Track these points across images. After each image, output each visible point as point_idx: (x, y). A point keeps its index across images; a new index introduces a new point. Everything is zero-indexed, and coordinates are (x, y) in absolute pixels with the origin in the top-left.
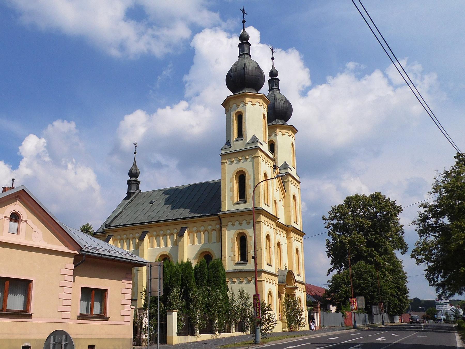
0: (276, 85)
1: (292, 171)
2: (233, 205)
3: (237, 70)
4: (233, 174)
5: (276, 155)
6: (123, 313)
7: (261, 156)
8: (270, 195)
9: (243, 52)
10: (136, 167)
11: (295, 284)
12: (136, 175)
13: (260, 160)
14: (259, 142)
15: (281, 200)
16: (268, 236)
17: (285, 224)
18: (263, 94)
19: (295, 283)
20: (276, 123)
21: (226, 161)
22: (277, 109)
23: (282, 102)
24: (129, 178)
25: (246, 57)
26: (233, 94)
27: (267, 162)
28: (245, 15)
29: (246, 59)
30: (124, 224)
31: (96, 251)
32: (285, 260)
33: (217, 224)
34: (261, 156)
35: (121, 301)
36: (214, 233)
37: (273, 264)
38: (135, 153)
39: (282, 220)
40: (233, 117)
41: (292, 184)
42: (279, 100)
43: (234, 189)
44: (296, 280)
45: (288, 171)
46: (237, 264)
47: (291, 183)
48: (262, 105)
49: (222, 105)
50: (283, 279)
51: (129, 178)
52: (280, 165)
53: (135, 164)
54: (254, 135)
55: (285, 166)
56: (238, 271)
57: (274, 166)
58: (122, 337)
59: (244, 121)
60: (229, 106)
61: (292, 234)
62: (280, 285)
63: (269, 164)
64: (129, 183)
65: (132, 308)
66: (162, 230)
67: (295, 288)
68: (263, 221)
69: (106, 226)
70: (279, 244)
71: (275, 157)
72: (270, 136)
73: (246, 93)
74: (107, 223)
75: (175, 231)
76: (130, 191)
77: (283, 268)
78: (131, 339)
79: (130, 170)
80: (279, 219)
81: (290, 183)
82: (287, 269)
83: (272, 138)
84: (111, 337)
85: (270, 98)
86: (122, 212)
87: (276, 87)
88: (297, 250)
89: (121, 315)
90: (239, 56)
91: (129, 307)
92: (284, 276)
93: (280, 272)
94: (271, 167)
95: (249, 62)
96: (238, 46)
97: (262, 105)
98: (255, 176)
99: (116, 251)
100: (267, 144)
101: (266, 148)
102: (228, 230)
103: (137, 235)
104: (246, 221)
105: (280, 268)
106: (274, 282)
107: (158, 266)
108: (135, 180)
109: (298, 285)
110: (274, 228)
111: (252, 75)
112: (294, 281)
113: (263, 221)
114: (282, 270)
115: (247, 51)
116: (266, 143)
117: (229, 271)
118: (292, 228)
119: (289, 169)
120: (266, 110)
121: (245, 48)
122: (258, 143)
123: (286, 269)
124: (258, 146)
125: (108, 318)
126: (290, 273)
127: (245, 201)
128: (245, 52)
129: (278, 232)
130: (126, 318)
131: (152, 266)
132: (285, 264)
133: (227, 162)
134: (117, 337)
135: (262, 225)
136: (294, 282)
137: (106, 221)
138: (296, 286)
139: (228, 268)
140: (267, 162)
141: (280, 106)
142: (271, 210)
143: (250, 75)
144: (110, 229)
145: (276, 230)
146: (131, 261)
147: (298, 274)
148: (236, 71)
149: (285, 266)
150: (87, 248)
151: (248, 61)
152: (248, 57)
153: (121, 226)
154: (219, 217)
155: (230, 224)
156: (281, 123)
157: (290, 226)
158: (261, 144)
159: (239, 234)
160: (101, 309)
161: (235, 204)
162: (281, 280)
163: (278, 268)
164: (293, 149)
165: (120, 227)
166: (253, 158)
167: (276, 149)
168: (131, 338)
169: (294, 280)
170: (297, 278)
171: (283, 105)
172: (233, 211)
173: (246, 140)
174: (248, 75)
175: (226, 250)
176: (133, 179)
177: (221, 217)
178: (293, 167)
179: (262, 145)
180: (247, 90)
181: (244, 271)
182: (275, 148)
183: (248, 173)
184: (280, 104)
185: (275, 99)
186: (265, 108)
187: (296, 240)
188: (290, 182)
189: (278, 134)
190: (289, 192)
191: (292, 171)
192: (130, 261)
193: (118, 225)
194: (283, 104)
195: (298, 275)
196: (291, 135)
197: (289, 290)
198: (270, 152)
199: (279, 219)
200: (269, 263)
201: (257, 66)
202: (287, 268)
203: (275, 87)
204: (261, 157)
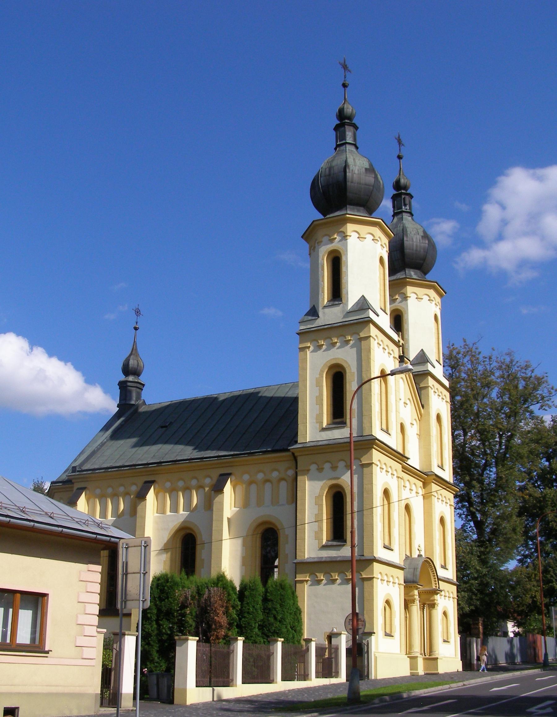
0: (405, 205)
1: (434, 367)
2: (320, 431)
3: (332, 172)
4: (322, 371)
5: (406, 337)
6: (81, 641)
7: (376, 336)
8: (391, 412)
9: (342, 140)
10: (137, 355)
11: (436, 584)
12: (137, 373)
13: (374, 344)
14: (372, 309)
15: (414, 422)
16: (386, 493)
17: (419, 469)
18: (380, 219)
19: (437, 583)
20: (405, 276)
21: (308, 344)
22: (408, 251)
23: (417, 238)
24: (123, 378)
25: (349, 149)
26: (323, 218)
27: (386, 348)
28: (348, 74)
29: (349, 152)
30: (108, 465)
31: (24, 515)
32: (419, 540)
33: (289, 468)
34: (376, 336)
35: (77, 617)
36: (283, 484)
37: (395, 545)
38: (136, 329)
39: (415, 462)
40: (323, 259)
41: (435, 392)
42: (413, 233)
43: (323, 400)
44: (439, 577)
45: (427, 367)
46: (324, 547)
47: (433, 390)
48: (379, 239)
49: (302, 237)
50: (415, 574)
51: (123, 378)
52: (412, 354)
53: (134, 351)
54: (363, 296)
55: (422, 358)
56: (328, 560)
57: (400, 357)
58: (77, 690)
59: (343, 269)
60: (316, 240)
61: (434, 487)
62: (407, 587)
63: (391, 352)
64: (123, 385)
65: (98, 632)
66: (195, 478)
67: (436, 592)
68: (378, 463)
69: (74, 469)
70: (407, 508)
71: (403, 339)
72: (392, 301)
73: (348, 216)
74: (76, 464)
75: (208, 481)
76: (123, 402)
77: (415, 555)
78: (96, 694)
79: (126, 360)
80: (409, 459)
81: (431, 392)
82: (421, 555)
83: (397, 305)
84: (54, 690)
85: (396, 229)
86: (105, 442)
87: (407, 209)
88: (442, 520)
89: (76, 646)
90: (335, 147)
91: (93, 631)
92: (417, 568)
93: (408, 561)
94: (395, 358)
95: (354, 159)
96: (334, 129)
97: (379, 239)
98: (363, 375)
99: (68, 516)
100: (387, 314)
101: (384, 321)
102: (310, 479)
103: (208, 481)
104: (344, 462)
105: (408, 554)
106: (397, 581)
107: (141, 546)
108: (134, 381)
109: (443, 585)
110: (398, 477)
111: (360, 184)
112: (434, 576)
113: (378, 463)
114: (413, 558)
115: (351, 139)
116: (385, 311)
117: (308, 561)
118: (434, 477)
119: (428, 363)
120: (386, 249)
121: (347, 133)
122: (370, 310)
123: (420, 556)
124: (369, 317)
125: (47, 652)
126: (429, 563)
127: (343, 424)
128: (348, 140)
129: (407, 484)
130: (87, 653)
131: (129, 547)
132: (419, 546)
133: (309, 347)
134: (66, 690)
135: (376, 470)
136: (435, 581)
137: (75, 460)
138: (439, 588)
139: (309, 553)
140: (386, 348)
141: (413, 244)
142: (393, 441)
143: (355, 183)
144: (82, 476)
145: (402, 480)
146: (98, 536)
147: (443, 564)
148: (330, 175)
149: (418, 550)
150: (3, 506)
151: (352, 157)
152: (352, 150)
153: (103, 471)
154: (293, 454)
155: (313, 467)
156: (414, 277)
157: (429, 473)
158: (375, 313)
159: (331, 487)
160: (33, 632)
161: (323, 429)
162: (410, 577)
163: (406, 555)
164: (436, 327)
165: (113, 470)
166: (361, 339)
167: (405, 326)
168: (97, 692)
169: (436, 577)
170: (441, 573)
171: (419, 244)
172: (320, 443)
173: (347, 305)
174: (352, 182)
175: (305, 519)
176: (131, 378)
177: (296, 454)
178: (437, 360)
179: (378, 316)
180: (350, 210)
181: (338, 559)
182: (404, 324)
183: (350, 369)
184: (413, 241)
185: (404, 230)
186: (384, 246)
187: (440, 501)
188: (432, 389)
189: (410, 297)
190: (428, 408)
191: (434, 367)
192: (108, 538)
193: (96, 467)
194: (418, 241)
195: (444, 567)
196: (433, 301)
197: (424, 597)
198: (395, 331)
199: (408, 459)
200: (387, 545)
201: (368, 167)
202: (423, 553)
203: (403, 210)
204: (375, 338)
